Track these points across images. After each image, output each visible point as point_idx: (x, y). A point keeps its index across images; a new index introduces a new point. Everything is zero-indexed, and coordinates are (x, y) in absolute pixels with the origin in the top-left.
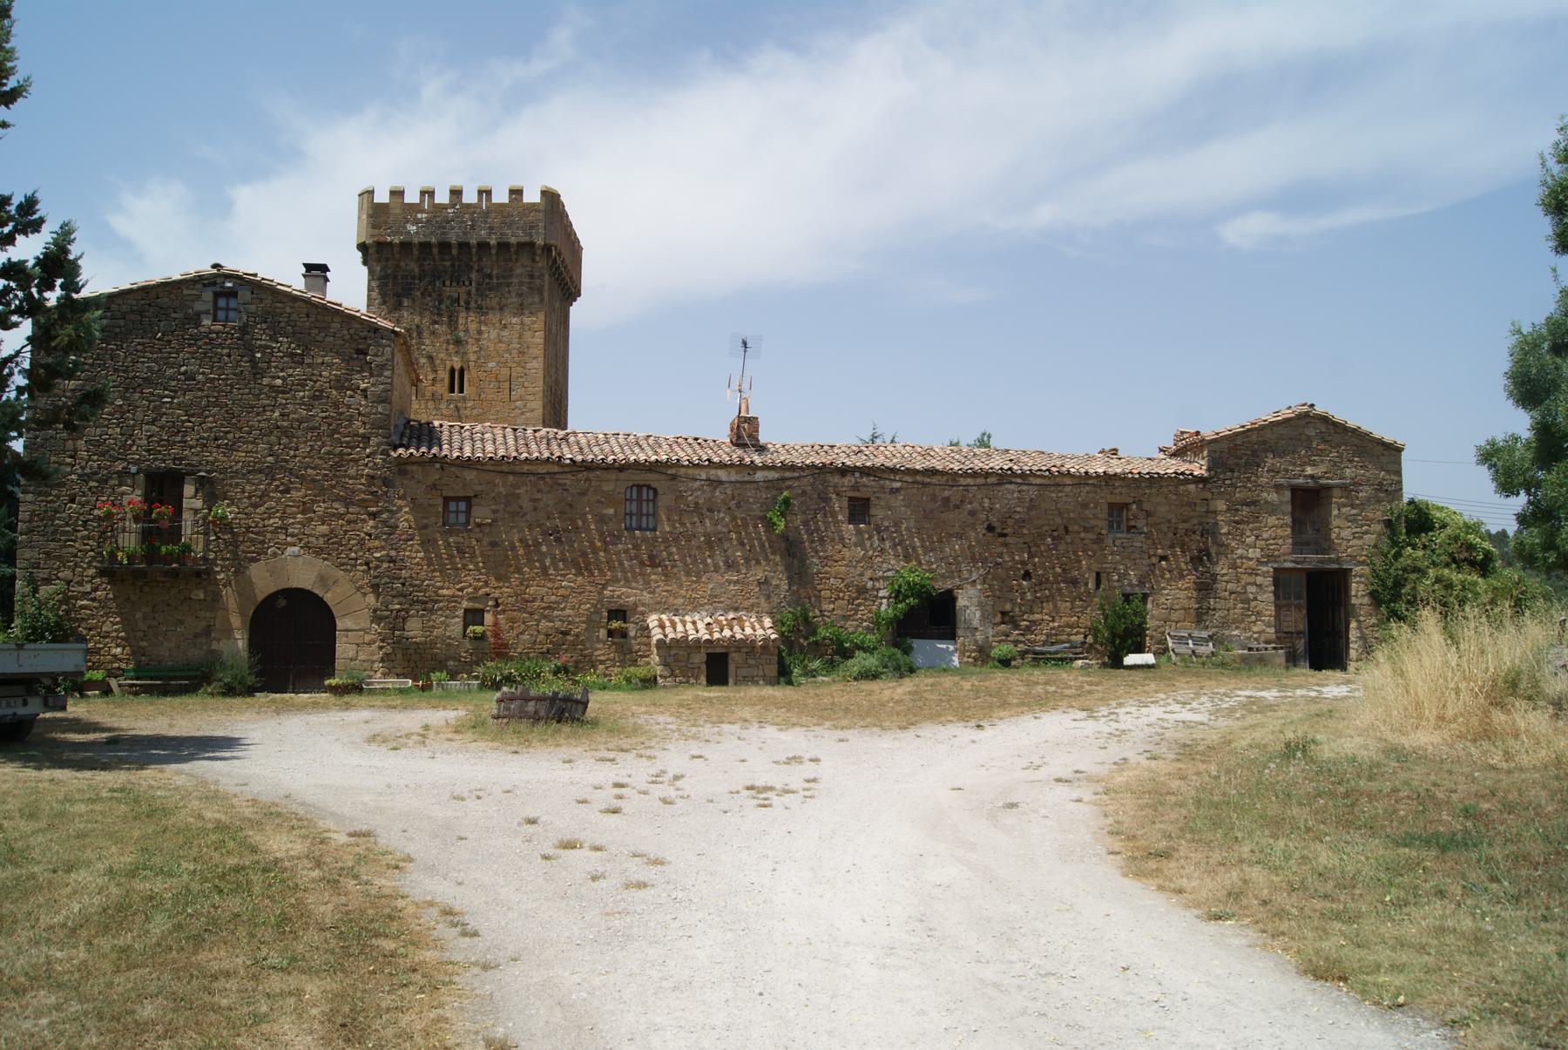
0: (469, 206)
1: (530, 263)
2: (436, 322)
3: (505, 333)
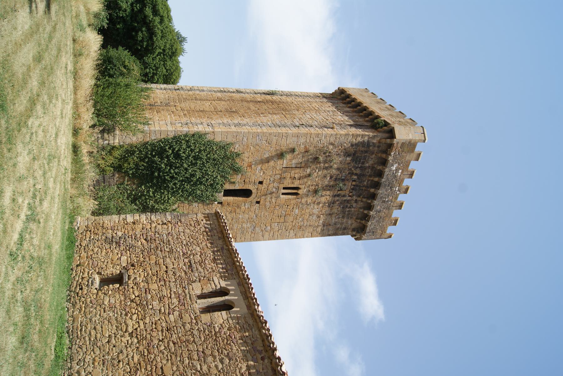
1: (353, 226)
2: (331, 177)
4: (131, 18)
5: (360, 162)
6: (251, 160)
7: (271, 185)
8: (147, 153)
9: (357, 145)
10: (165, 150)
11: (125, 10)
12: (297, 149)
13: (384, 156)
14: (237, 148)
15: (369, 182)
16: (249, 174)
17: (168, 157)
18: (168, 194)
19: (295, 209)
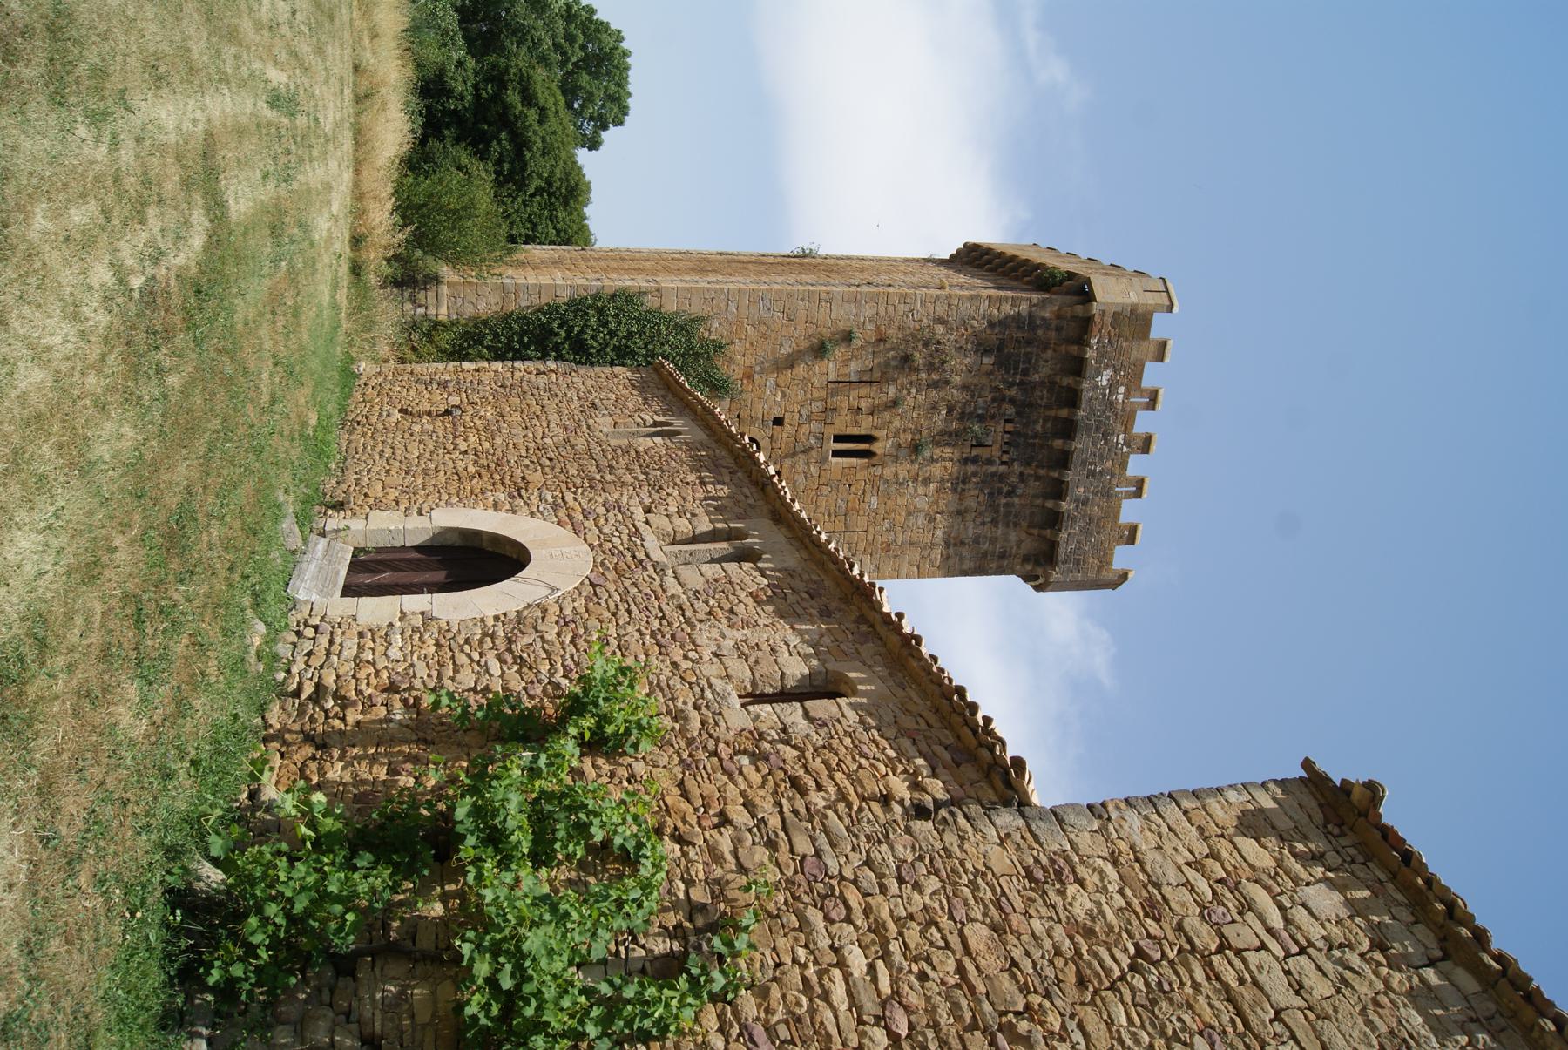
0: (1124, 466)
1: (1024, 550)
2: (950, 410)
3: (921, 520)
4: (475, 115)
5: (1016, 369)
7: (804, 429)
8: (510, 339)
9: (1004, 323)
11: (462, 98)
12: (857, 332)
13: (1074, 349)
14: (716, 330)
15: (1049, 425)
16: (748, 397)
19: (868, 494)
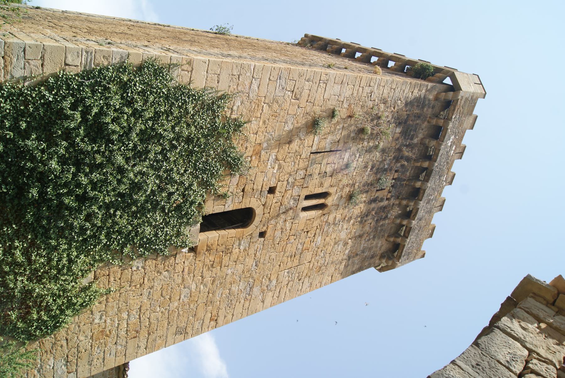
6: (260, 138)
10: (61, 115)
14: (236, 109)
17: (68, 135)
18: (70, 248)
